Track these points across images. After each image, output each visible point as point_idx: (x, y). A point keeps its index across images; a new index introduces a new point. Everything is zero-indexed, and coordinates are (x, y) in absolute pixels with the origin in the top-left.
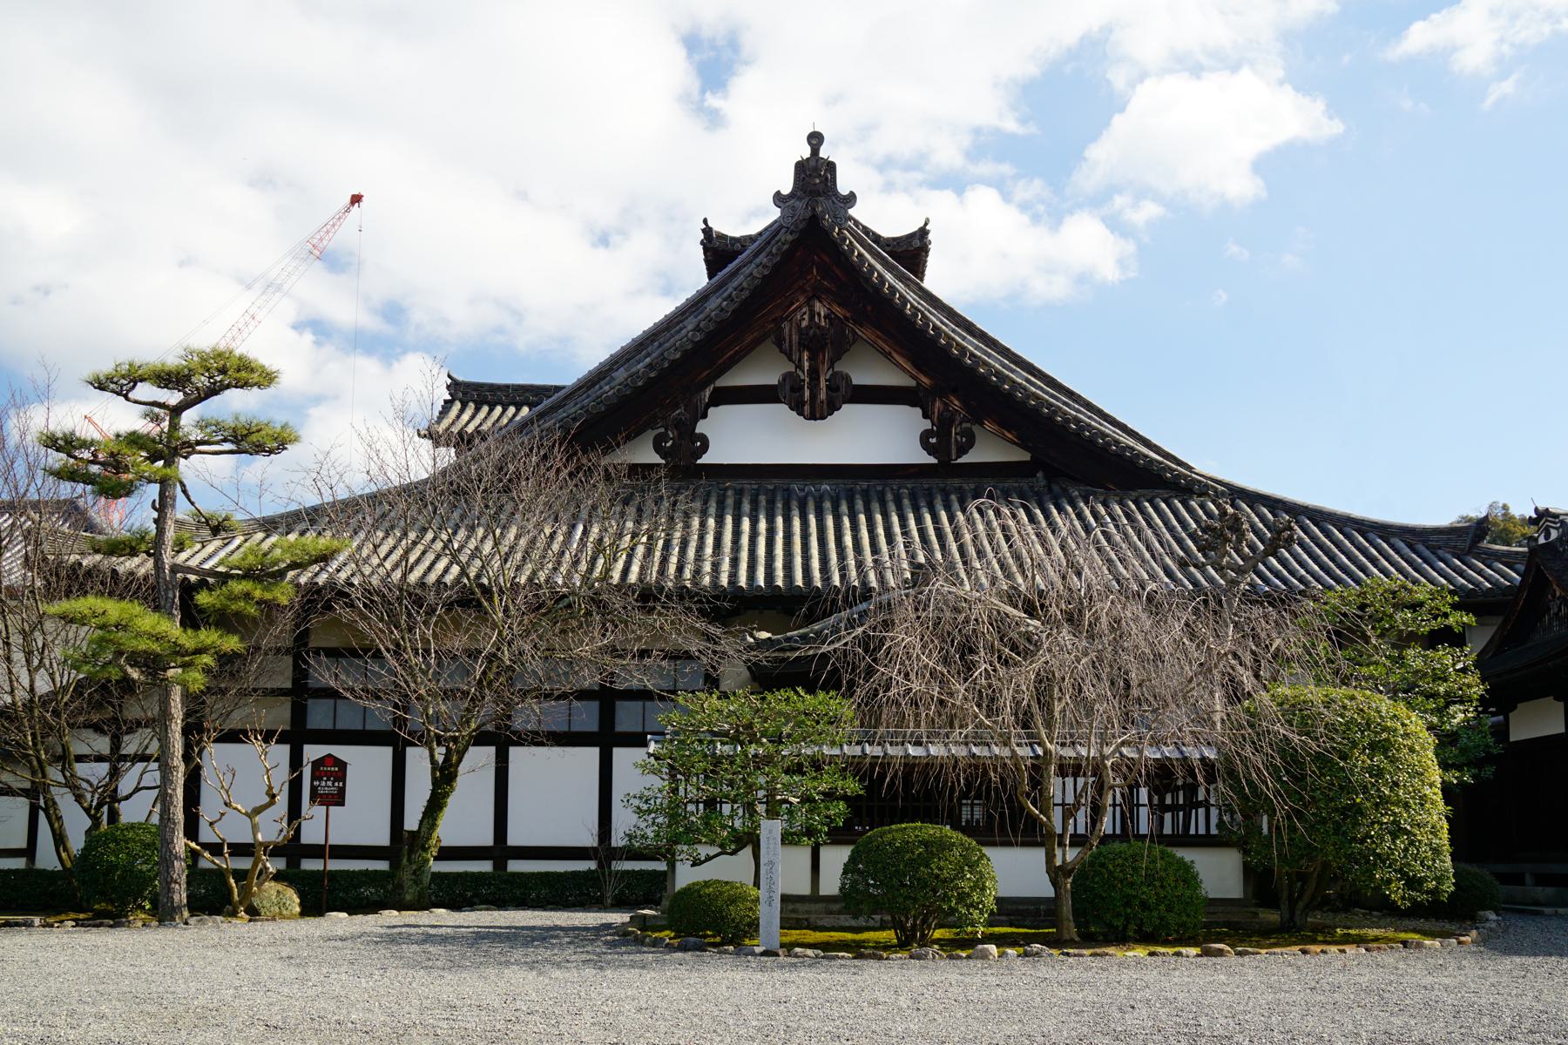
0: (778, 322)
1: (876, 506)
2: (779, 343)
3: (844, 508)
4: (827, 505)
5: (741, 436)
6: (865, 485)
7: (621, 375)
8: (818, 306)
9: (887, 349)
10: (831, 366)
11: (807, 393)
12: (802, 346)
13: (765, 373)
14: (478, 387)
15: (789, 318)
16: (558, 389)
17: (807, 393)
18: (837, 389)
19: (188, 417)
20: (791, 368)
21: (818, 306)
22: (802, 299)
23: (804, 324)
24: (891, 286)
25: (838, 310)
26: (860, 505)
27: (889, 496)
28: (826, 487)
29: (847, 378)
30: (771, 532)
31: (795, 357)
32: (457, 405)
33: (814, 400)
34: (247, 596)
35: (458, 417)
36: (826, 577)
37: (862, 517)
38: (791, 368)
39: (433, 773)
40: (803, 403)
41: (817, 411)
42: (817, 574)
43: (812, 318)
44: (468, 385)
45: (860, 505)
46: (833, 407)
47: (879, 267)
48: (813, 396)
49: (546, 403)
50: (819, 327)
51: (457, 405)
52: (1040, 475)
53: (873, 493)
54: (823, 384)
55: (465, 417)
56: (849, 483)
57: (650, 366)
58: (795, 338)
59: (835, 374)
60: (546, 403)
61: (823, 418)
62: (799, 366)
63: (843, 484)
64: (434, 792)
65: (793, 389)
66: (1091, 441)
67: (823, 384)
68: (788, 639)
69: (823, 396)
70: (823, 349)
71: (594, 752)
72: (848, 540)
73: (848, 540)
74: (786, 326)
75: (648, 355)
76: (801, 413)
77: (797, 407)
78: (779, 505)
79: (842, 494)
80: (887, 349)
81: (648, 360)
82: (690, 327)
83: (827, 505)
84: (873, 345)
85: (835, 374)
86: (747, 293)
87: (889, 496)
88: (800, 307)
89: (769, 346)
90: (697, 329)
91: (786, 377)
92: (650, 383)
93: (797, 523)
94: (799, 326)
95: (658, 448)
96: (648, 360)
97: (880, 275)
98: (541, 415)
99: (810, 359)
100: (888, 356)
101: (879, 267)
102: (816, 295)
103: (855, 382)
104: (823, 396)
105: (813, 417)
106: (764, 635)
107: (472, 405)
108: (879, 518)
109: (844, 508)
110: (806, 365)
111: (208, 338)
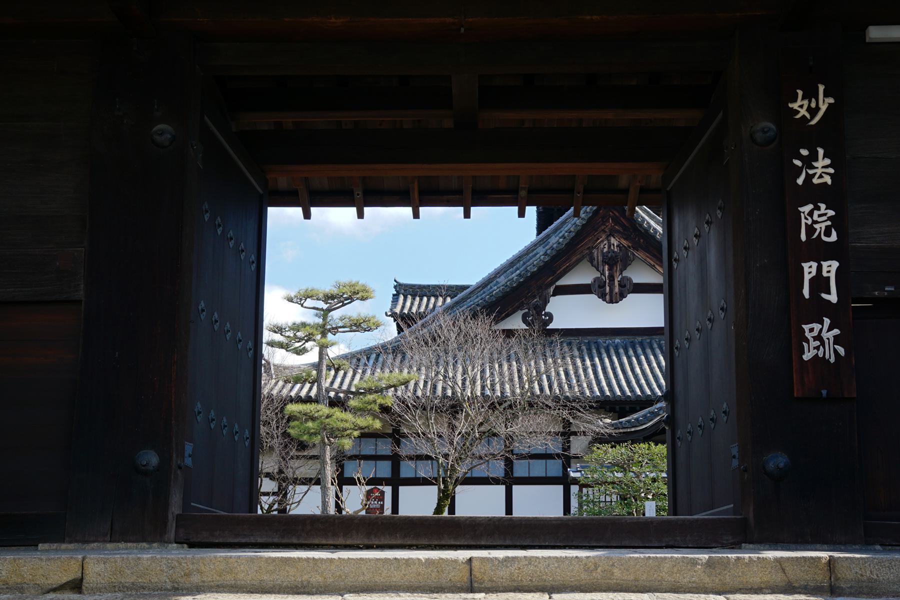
0: (590, 249)
1: (649, 351)
2: (591, 261)
3: (631, 352)
4: (621, 351)
5: (569, 312)
6: (640, 339)
7: (502, 280)
8: (613, 240)
9: (652, 263)
10: (621, 273)
11: (608, 289)
12: (605, 262)
13: (583, 276)
14: (412, 286)
15: (597, 247)
16: (463, 288)
17: (608, 289)
18: (625, 286)
19: (336, 315)
20: (598, 275)
21: (613, 240)
22: (604, 237)
23: (605, 250)
24: (654, 229)
25: (624, 242)
26: (639, 351)
27: (655, 346)
28: (617, 341)
29: (630, 280)
30: (594, 366)
31: (601, 269)
32: (401, 298)
33: (612, 291)
34: (375, 402)
35: (404, 303)
36: (632, 390)
37: (643, 357)
38: (598, 275)
39: (439, 494)
40: (606, 295)
41: (614, 299)
42: (606, 388)
43: (609, 247)
44: (406, 285)
45: (639, 351)
46: (622, 296)
47: (647, 218)
48: (611, 290)
49: (460, 296)
50: (614, 252)
51: (401, 298)
52: (807, 356)
53: (645, 344)
54: (616, 283)
55: (408, 304)
56: (631, 339)
57: (520, 275)
58: (600, 258)
59: (623, 278)
60: (460, 296)
61: (617, 302)
62: (603, 274)
63: (628, 339)
64: (438, 504)
65: (600, 287)
66: (647, 231)
67: (616, 283)
68: (621, 423)
69: (617, 290)
70: (616, 264)
71: (502, 488)
72: (638, 370)
73: (638, 370)
74: (595, 251)
75: (517, 269)
76: (604, 300)
77: (602, 296)
78: (594, 351)
79: (628, 345)
80: (652, 263)
81: (518, 272)
82: (541, 253)
83: (621, 351)
84: (644, 261)
85: (623, 278)
86: (573, 234)
87: (655, 346)
88: (602, 241)
89: (585, 264)
90: (545, 254)
91: (595, 280)
92: (520, 285)
93: (607, 361)
94: (602, 251)
95: (525, 321)
96: (518, 272)
97: (648, 223)
98: (457, 304)
99: (609, 270)
100: (653, 267)
101: (647, 218)
102: (611, 234)
103: (635, 281)
104: (617, 290)
105: (611, 302)
106: (608, 421)
107: (409, 297)
108: (652, 357)
109: (631, 352)
110: (607, 273)
111: (346, 278)
